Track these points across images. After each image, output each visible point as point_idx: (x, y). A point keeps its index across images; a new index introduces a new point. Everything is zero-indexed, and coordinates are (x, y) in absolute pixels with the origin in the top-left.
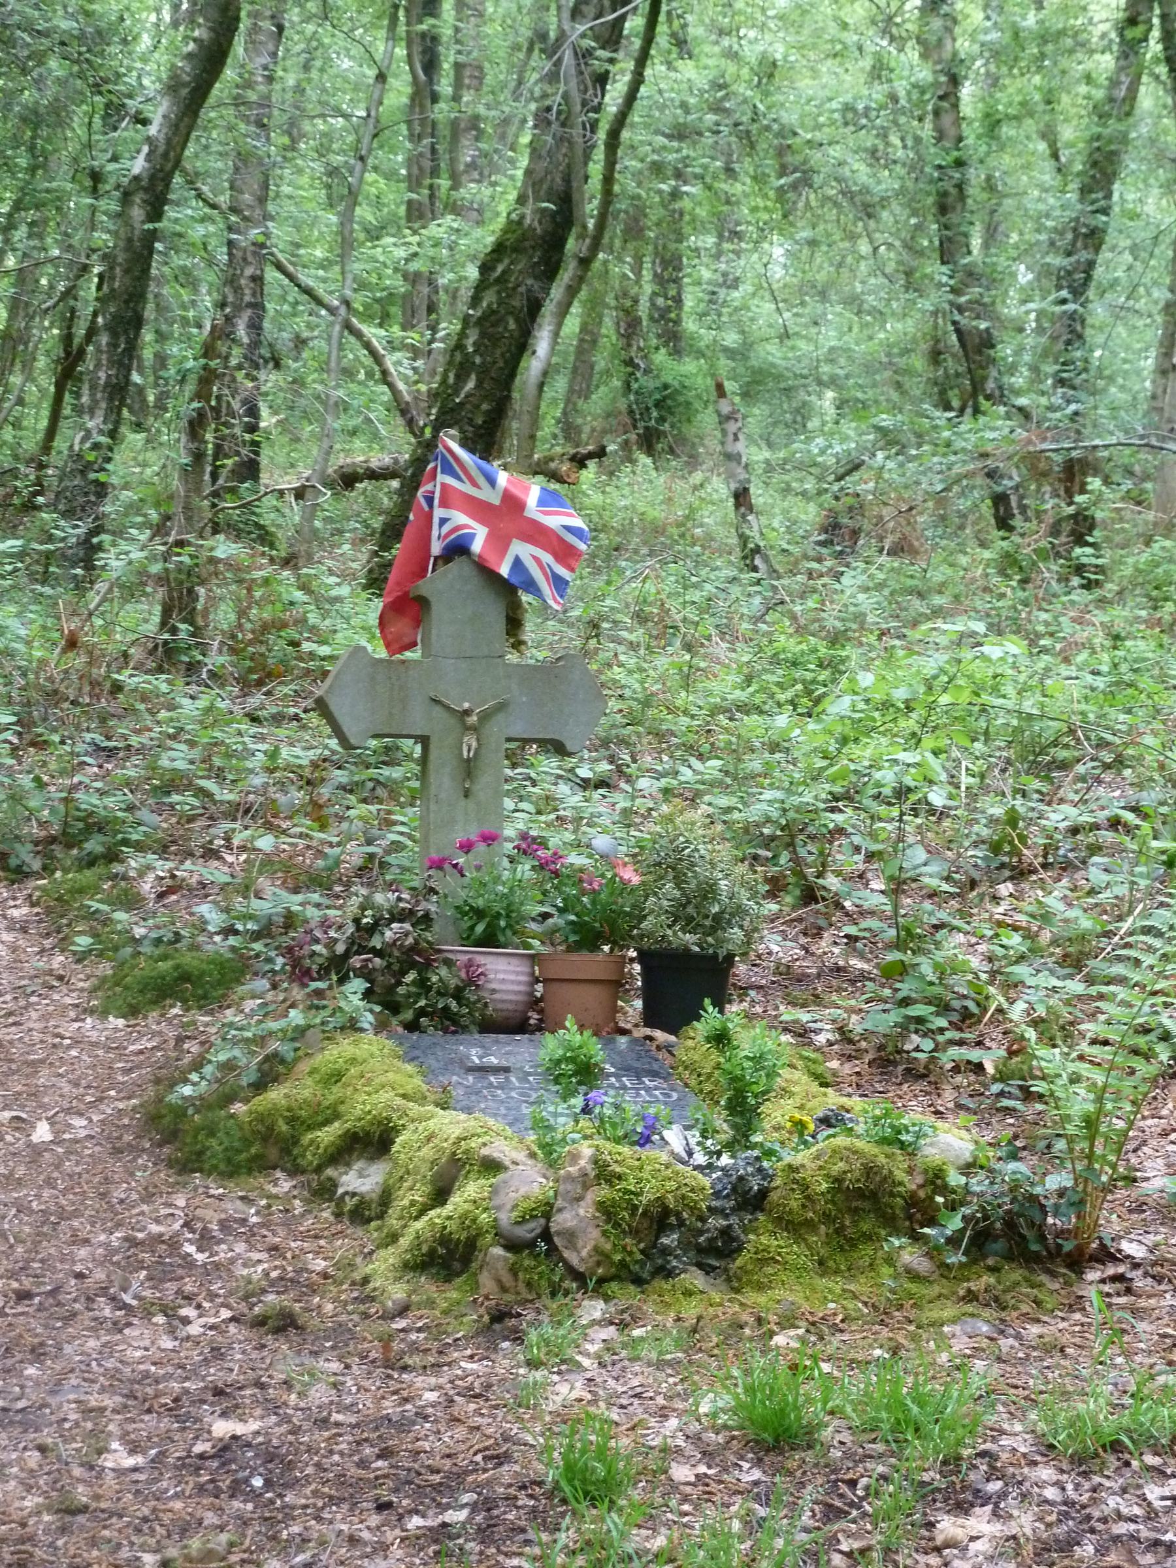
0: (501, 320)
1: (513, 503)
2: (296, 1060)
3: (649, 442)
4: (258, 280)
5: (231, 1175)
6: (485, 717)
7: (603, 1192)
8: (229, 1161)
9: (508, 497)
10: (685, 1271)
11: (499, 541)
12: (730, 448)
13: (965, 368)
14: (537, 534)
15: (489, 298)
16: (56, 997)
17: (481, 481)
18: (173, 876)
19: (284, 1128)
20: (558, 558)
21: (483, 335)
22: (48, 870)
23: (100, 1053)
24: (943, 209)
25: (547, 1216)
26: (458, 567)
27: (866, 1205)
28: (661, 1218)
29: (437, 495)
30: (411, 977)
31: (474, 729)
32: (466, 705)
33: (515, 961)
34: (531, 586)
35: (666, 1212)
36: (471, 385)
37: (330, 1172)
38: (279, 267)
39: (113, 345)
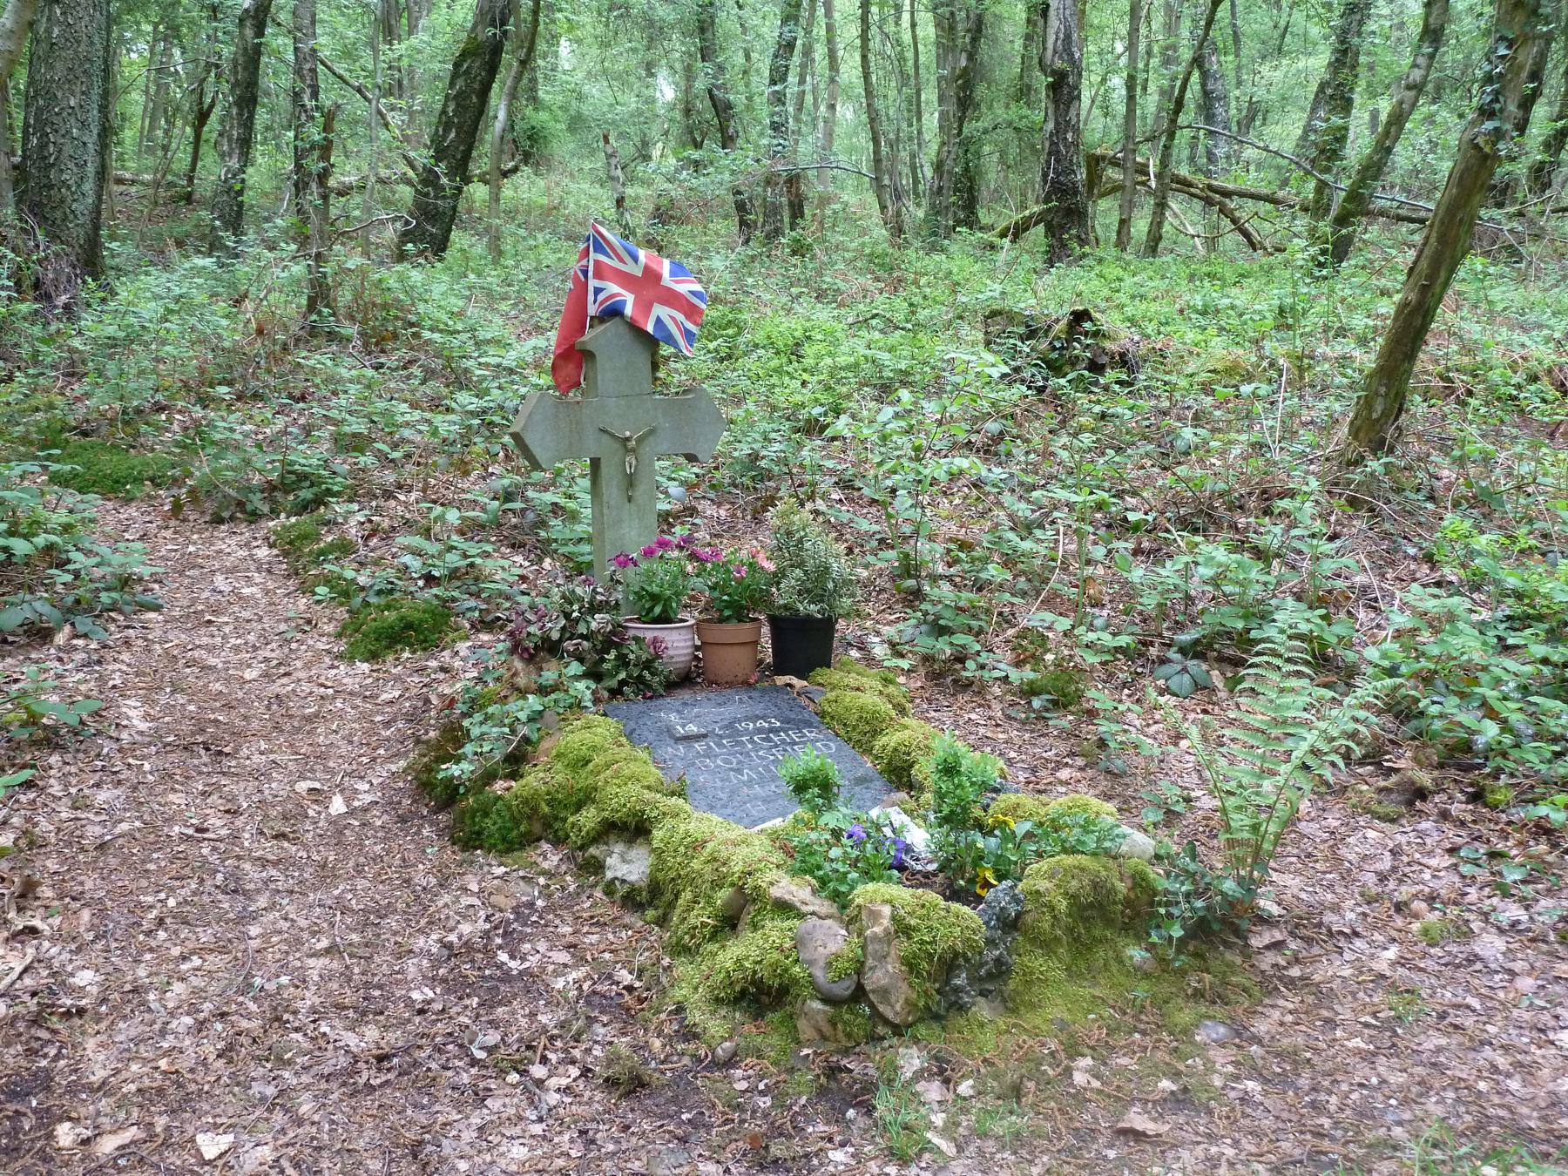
0: (468, 97)
1: (651, 276)
2: (540, 739)
3: (527, 158)
4: (313, 71)
5: (509, 850)
6: (640, 440)
7: (903, 947)
8: (504, 839)
9: (647, 269)
10: (974, 1004)
11: (645, 307)
12: (613, 173)
13: (711, 121)
14: (672, 299)
15: (460, 83)
16: (311, 642)
17: (627, 258)
18: (370, 521)
19: (546, 809)
20: (688, 317)
21: (458, 105)
22: (275, 513)
23: (358, 702)
24: (702, 30)
25: (859, 972)
26: (610, 325)
27: (1095, 913)
28: (949, 964)
29: (591, 269)
30: (612, 655)
31: (633, 450)
32: (628, 434)
33: (683, 632)
34: (670, 340)
35: (956, 955)
36: (453, 135)
37: (592, 850)
38: (323, 63)
39: (240, 114)
